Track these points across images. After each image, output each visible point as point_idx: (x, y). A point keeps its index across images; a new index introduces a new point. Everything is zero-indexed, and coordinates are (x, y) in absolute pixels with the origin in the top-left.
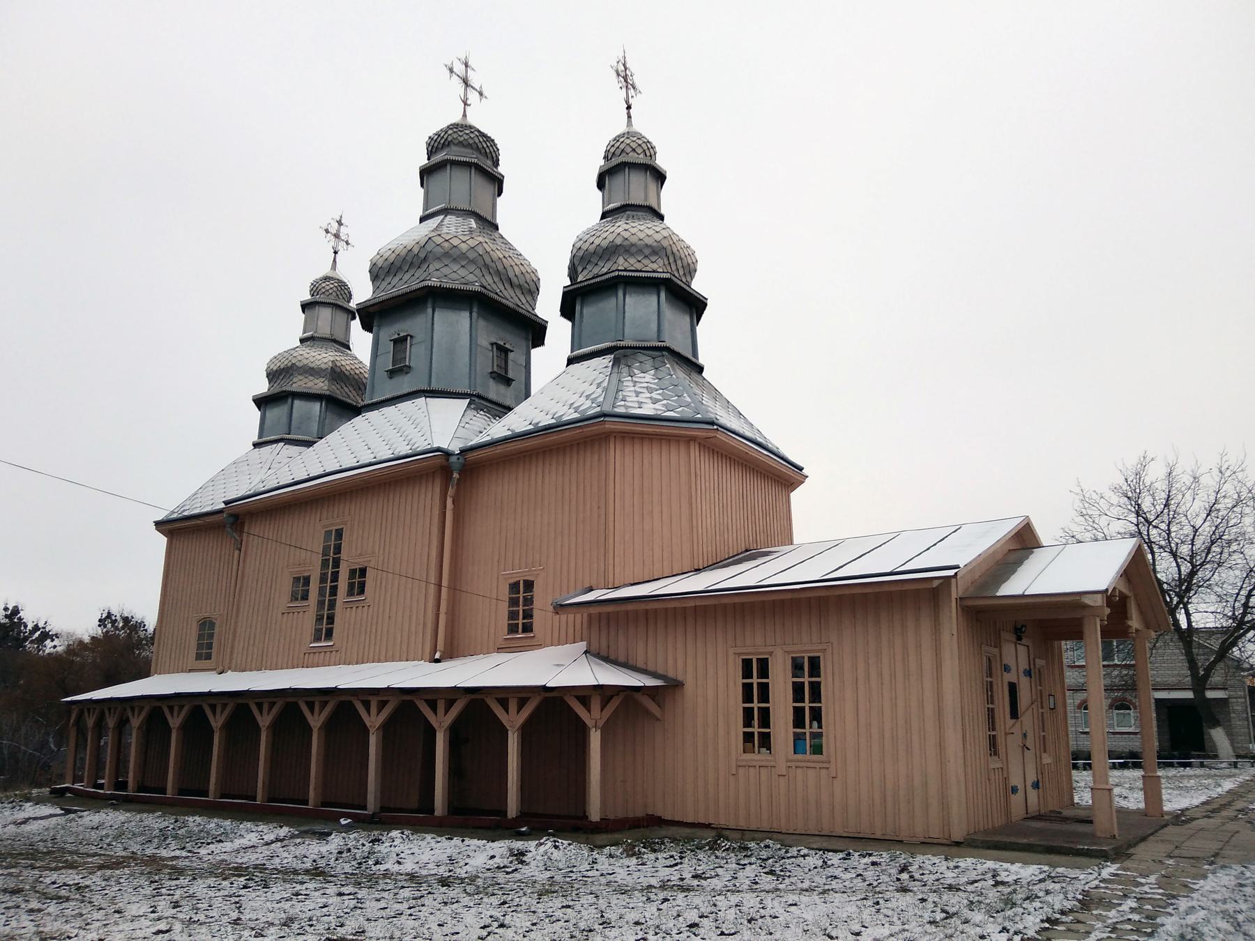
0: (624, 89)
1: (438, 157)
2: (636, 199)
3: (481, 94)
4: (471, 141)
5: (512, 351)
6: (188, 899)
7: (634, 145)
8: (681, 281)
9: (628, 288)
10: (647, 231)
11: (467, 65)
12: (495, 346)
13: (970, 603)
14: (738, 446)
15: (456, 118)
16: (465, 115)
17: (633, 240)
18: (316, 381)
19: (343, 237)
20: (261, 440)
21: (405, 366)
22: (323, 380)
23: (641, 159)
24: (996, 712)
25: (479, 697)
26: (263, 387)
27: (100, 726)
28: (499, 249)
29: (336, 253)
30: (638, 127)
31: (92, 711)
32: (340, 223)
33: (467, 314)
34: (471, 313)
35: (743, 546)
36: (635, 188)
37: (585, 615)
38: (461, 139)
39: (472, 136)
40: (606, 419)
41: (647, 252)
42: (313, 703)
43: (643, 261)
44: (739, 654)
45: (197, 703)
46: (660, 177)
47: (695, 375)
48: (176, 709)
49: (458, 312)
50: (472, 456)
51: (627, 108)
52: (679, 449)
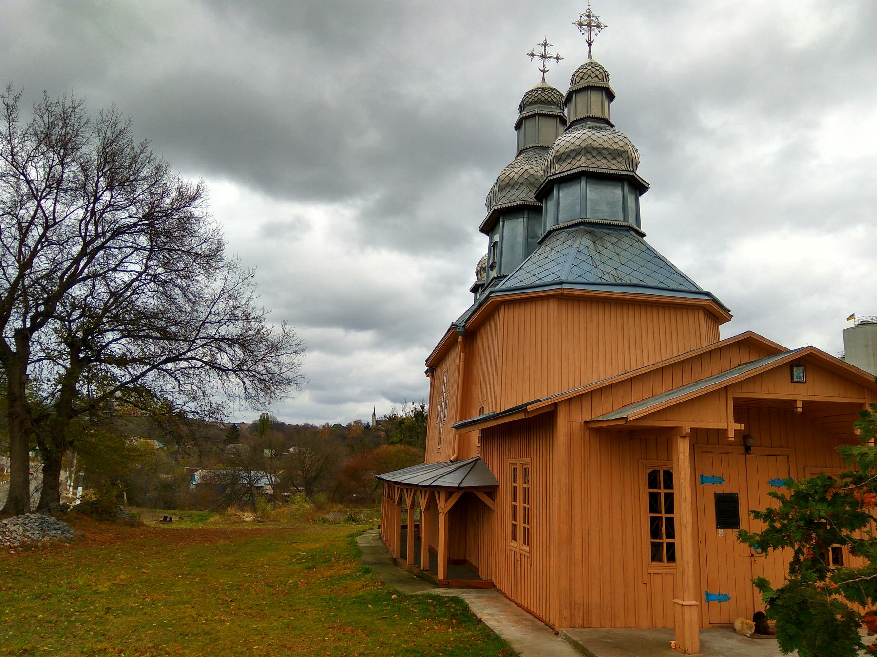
0: (587, 34)
2: (595, 112)
4: (543, 99)
8: (612, 169)
9: (562, 186)
14: (613, 296)
16: (543, 80)
23: (597, 83)
26: (473, 280)
29: (590, 45)
30: (596, 59)
38: (530, 100)
39: (550, 95)
41: (573, 155)
46: (611, 96)
47: (626, 241)
49: (516, 220)
51: (588, 46)
52: (670, 312)
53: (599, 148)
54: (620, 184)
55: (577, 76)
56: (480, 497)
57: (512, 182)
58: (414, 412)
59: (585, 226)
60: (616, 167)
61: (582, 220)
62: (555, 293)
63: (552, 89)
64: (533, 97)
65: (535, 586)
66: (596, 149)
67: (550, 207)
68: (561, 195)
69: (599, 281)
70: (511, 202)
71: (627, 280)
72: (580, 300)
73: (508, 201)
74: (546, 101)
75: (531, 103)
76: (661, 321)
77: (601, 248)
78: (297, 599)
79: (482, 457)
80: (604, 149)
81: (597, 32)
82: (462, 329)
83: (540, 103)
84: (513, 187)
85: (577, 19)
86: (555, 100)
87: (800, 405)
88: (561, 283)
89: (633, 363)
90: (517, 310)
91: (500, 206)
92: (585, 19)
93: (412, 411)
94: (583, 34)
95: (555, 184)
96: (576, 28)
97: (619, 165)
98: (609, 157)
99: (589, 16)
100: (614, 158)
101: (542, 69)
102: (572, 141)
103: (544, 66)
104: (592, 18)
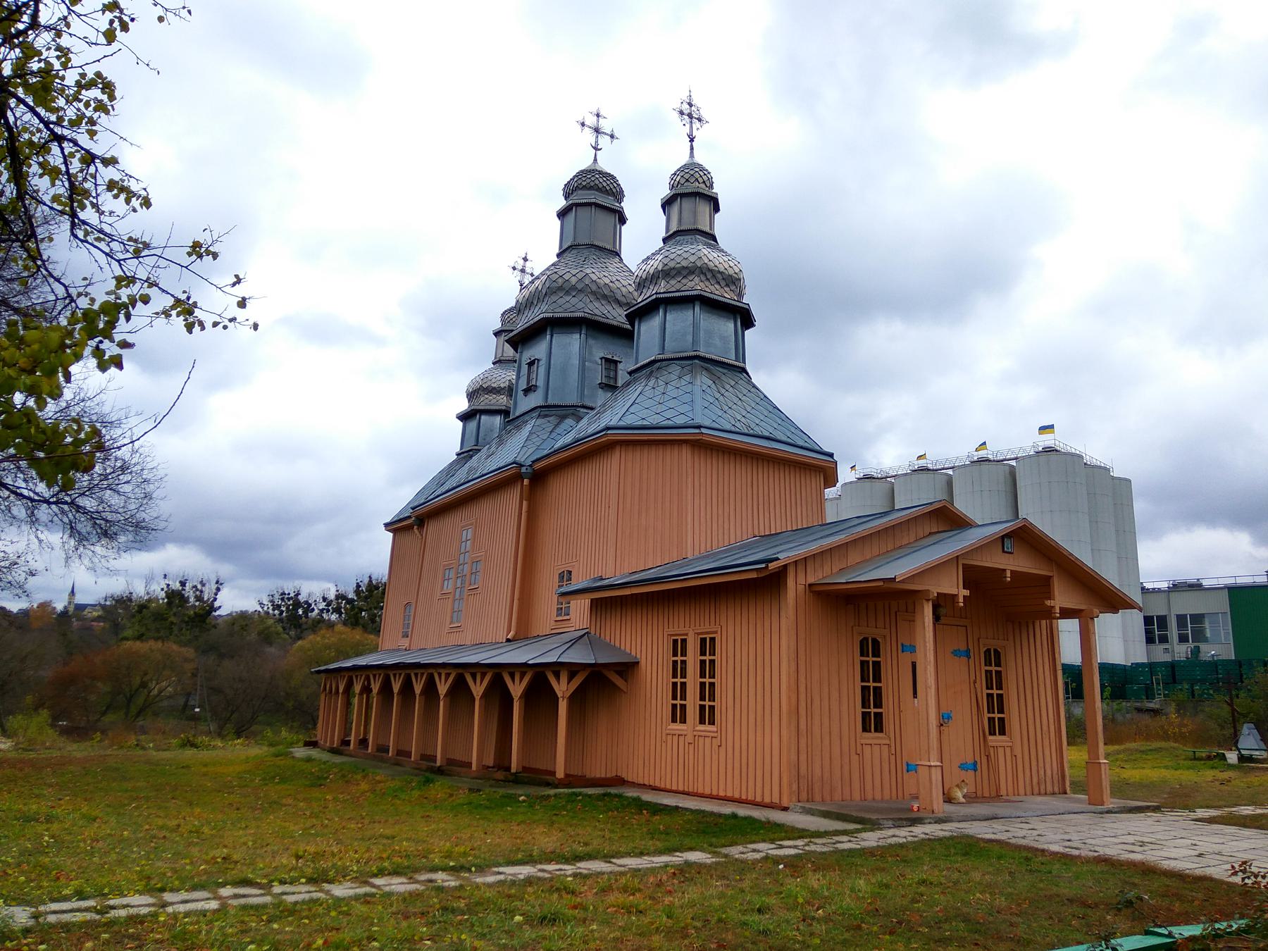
0: (688, 126)
1: (575, 199)
3: (612, 136)
5: (620, 362)
6: (385, 841)
7: (697, 175)
9: (668, 308)
10: (691, 251)
11: (598, 115)
12: (603, 360)
15: (586, 163)
16: (595, 160)
17: (672, 264)
19: (528, 270)
20: (463, 450)
25: (596, 669)
26: (463, 405)
29: (692, 140)
30: (699, 158)
31: (443, 677)
32: (525, 259)
33: (731, 325)
38: (584, 183)
39: (608, 183)
40: (609, 432)
41: (685, 273)
43: (682, 281)
44: (699, 634)
45: (497, 671)
47: (729, 379)
49: (570, 335)
56: (611, 678)
57: (567, 286)
58: (166, 589)
60: (727, 296)
63: (610, 175)
64: (588, 181)
65: (744, 761)
66: (711, 271)
67: (648, 330)
68: (667, 318)
69: (733, 429)
70: (565, 311)
71: (758, 431)
75: (584, 188)
77: (723, 391)
78: (327, 819)
81: (699, 126)
82: (530, 470)
83: (596, 190)
84: (567, 293)
86: (614, 190)
88: (699, 427)
89: (778, 527)
90: (646, 451)
92: (686, 108)
93: (162, 589)
95: (661, 304)
98: (723, 283)
99: (690, 105)
100: (727, 285)
102: (685, 255)
103: (597, 142)
104: (693, 108)
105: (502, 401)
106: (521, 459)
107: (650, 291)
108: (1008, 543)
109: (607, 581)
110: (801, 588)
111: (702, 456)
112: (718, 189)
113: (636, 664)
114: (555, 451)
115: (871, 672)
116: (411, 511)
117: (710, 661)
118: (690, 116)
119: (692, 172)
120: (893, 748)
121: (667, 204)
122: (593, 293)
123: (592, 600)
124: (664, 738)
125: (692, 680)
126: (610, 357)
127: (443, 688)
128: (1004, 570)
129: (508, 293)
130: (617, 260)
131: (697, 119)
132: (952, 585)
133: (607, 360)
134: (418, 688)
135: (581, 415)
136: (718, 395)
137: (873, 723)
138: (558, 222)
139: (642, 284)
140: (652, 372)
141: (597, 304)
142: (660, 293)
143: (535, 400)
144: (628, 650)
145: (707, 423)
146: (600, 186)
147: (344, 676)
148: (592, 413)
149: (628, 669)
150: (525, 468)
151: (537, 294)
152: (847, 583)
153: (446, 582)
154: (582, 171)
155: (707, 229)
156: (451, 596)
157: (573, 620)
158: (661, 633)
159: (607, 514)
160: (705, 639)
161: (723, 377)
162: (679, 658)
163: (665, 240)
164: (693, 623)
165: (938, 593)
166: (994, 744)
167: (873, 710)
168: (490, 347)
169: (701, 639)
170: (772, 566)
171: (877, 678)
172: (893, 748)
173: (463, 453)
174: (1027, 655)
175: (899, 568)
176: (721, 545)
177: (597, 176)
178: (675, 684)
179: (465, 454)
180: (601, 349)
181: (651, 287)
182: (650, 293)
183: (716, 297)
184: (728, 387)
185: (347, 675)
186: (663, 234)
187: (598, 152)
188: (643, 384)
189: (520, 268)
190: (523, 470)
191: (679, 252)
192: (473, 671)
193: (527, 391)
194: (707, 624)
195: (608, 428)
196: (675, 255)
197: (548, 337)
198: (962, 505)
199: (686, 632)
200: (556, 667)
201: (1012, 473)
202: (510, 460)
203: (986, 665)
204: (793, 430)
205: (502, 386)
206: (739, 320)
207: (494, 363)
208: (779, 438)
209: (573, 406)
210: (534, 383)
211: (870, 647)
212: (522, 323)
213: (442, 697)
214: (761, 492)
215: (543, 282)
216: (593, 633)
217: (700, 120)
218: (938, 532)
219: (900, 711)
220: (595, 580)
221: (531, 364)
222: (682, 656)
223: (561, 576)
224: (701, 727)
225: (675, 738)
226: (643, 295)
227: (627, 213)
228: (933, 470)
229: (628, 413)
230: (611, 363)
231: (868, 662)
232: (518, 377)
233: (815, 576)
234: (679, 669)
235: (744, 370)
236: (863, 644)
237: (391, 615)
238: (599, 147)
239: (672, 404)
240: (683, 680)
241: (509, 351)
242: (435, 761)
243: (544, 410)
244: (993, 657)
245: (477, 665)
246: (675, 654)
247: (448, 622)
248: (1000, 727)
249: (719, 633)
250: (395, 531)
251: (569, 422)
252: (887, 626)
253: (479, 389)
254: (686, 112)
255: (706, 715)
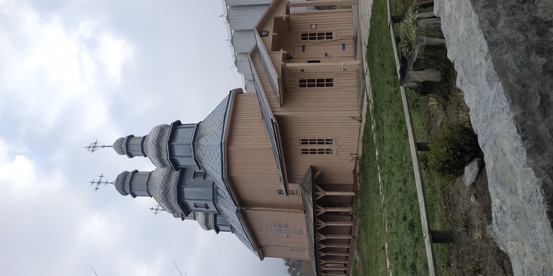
0: (98, 148)
5: (195, 171)
11: (93, 182)
12: (194, 178)
13: (282, 104)
15: (113, 187)
16: (111, 183)
17: (156, 154)
18: (210, 218)
19: (157, 208)
20: (231, 231)
21: (205, 205)
22: (209, 216)
24: (319, 138)
26: (213, 231)
27: (324, 250)
28: (159, 178)
29: (104, 146)
32: (152, 209)
33: (180, 130)
34: (184, 187)
35: (261, 123)
36: (135, 146)
37: (289, 184)
38: (122, 187)
40: (224, 178)
42: (318, 226)
44: (300, 145)
47: (202, 131)
48: (318, 225)
50: (237, 204)
53: (158, 137)
54: (172, 146)
55: (120, 150)
59: (194, 142)
60: (168, 132)
61: (192, 144)
62: (226, 148)
64: (120, 186)
66: (158, 139)
67: (182, 162)
69: (222, 130)
71: (222, 120)
72: (230, 138)
73: (174, 196)
74: (124, 179)
76: (240, 112)
77: (206, 133)
79: (299, 182)
80: (158, 135)
82: (239, 207)
83: (124, 183)
85: (90, 152)
86: (124, 175)
87: (274, 34)
88: (221, 144)
91: (176, 199)
94: (98, 149)
96: (94, 152)
97: (167, 130)
98: (163, 133)
99: (90, 147)
100: (164, 132)
101: (105, 184)
103: (104, 183)
104: (91, 146)
105: (211, 217)
106: (235, 211)
107: (166, 162)
108: (263, 34)
109: (281, 177)
110: (282, 110)
111: (233, 142)
112: (125, 136)
113: (312, 166)
114: (232, 198)
115: (313, 36)
116: (256, 251)
117: (310, 141)
118: (94, 147)
119: (118, 146)
120: (338, 75)
121: (131, 156)
122: (167, 183)
123: (289, 183)
124: (338, 156)
125: (317, 147)
126: (193, 175)
127: (323, 238)
128: (273, 35)
129: (167, 216)
130: (152, 173)
131: (95, 144)
132: (279, 55)
133: (194, 176)
134: (324, 246)
135: (216, 186)
136: (208, 136)
137: (329, 83)
138: (137, 197)
139: (164, 165)
140: (199, 161)
141: (171, 181)
142: (168, 158)
143: (211, 204)
144: (307, 169)
145: (220, 140)
146: (122, 181)
147: (320, 274)
148: (216, 182)
149: (313, 170)
150: (238, 209)
151: (167, 205)
152: (280, 94)
153: (283, 236)
154: (117, 189)
155: (141, 140)
156: (288, 234)
157: (296, 189)
158: (300, 158)
159: (255, 178)
160: (302, 142)
161: (201, 133)
162: (309, 151)
163: (146, 156)
164: (295, 140)
165: (282, 61)
166: (335, 37)
167: (325, 82)
168: (189, 222)
169: (302, 144)
170: (274, 122)
171: (314, 81)
172: (338, 75)
173: (232, 231)
174: (304, 26)
175: (275, 77)
176: (265, 130)
177: (118, 182)
178: (319, 153)
179: (232, 230)
180: (189, 179)
181: (165, 161)
182: (168, 162)
183: (169, 136)
184: (205, 131)
185: (319, 273)
186: (143, 157)
187: (108, 182)
188: (204, 164)
189: (156, 211)
190: (239, 209)
191: (151, 151)
192: (317, 227)
193: (207, 207)
194: (297, 153)
195: (223, 179)
196: (152, 153)
197: (185, 200)
198: (249, 50)
199: (300, 150)
200: (314, 196)
201: (237, 31)
202: (235, 214)
203: (307, 40)
204: (221, 106)
205: (204, 216)
206: (178, 127)
207: (195, 220)
208: (225, 112)
209: (213, 189)
210: (204, 205)
211: (303, 83)
212: (180, 211)
213: (327, 238)
214: (245, 119)
215: (162, 203)
216: (301, 182)
217: (96, 143)
218: (259, 57)
219: (325, 72)
220: (281, 181)
221: (196, 207)
222: (308, 151)
223: (281, 193)
224: (334, 143)
225: (338, 152)
226: (168, 165)
227: (133, 170)
228: (232, 37)
229: (216, 171)
230: (195, 175)
231: (308, 84)
232: (201, 211)
233: (277, 105)
234: (313, 152)
235: (198, 125)
236: (301, 86)
237: (296, 256)
238: (106, 182)
239: (212, 153)
240: (317, 150)
241: (191, 214)
242: (350, 239)
243: (215, 201)
244: (304, 37)
245: (314, 225)
246: (308, 153)
247: (299, 235)
248: (329, 35)
249: (299, 138)
250: (264, 256)
251: (219, 191)
252: (295, 77)
253: (206, 226)
254: (93, 149)
255: (329, 142)
